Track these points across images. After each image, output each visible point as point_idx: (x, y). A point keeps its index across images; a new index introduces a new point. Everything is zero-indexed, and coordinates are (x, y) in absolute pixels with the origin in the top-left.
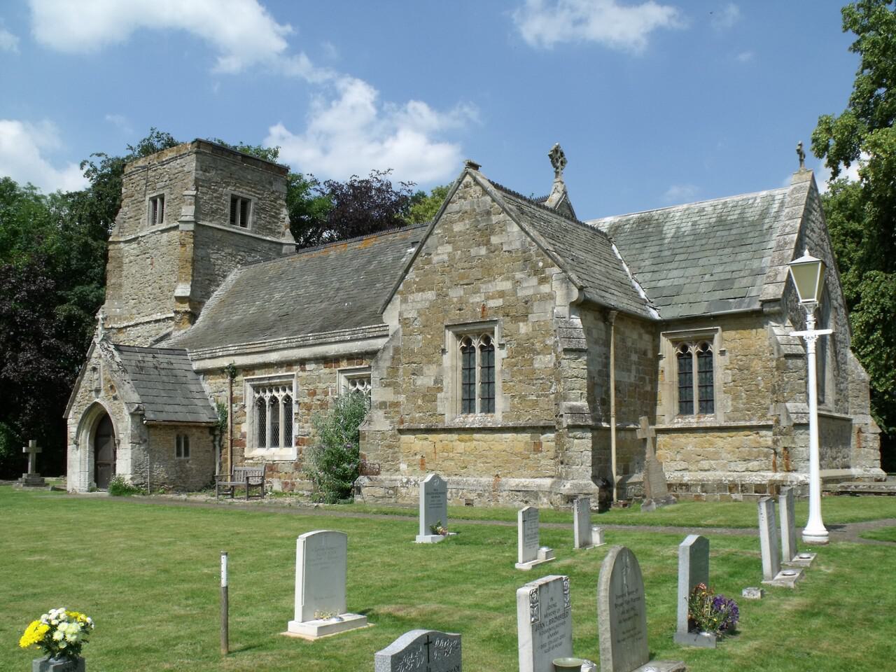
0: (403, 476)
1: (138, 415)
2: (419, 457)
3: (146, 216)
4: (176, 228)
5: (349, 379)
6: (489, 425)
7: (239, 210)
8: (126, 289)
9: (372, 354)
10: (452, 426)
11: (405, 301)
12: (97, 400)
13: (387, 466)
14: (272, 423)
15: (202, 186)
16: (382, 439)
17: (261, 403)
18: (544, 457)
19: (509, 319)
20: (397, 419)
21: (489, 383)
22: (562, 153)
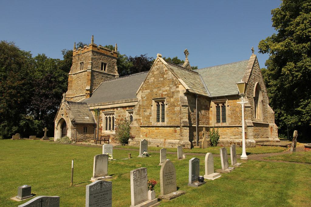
1: (73, 122)
2: (145, 134)
3: (79, 68)
4: (86, 71)
7: (104, 65)
8: (73, 88)
9: (134, 106)
10: (154, 125)
11: (142, 92)
12: (62, 117)
13: (137, 136)
16: (136, 129)
20: (140, 123)
21: (163, 114)
22: (188, 52)
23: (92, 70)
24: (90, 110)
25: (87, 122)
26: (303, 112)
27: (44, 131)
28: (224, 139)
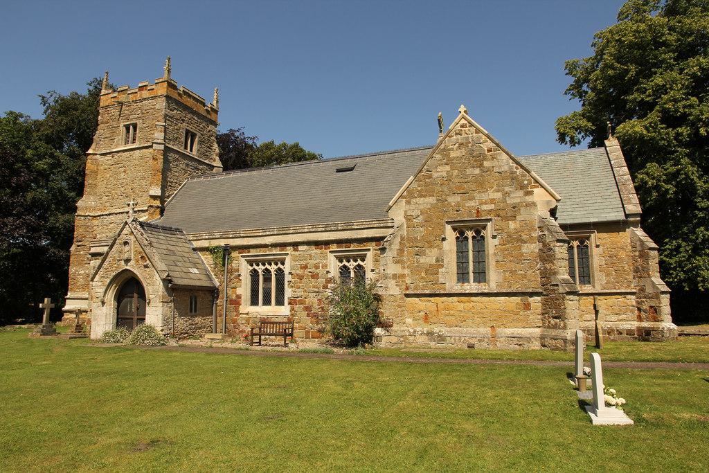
0: (406, 327)
1: (167, 281)
5: (337, 257)
6: (486, 291)
8: (101, 187)
10: (453, 292)
11: (408, 203)
14: (263, 288)
15: (169, 120)
16: (395, 301)
17: (254, 274)
18: (532, 314)
19: (500, 218)
23: (166, 147)
24: (194, 249)
25: (198, 283)
26: (671, 264)
27: (43, 309)
28: (589, 323)
